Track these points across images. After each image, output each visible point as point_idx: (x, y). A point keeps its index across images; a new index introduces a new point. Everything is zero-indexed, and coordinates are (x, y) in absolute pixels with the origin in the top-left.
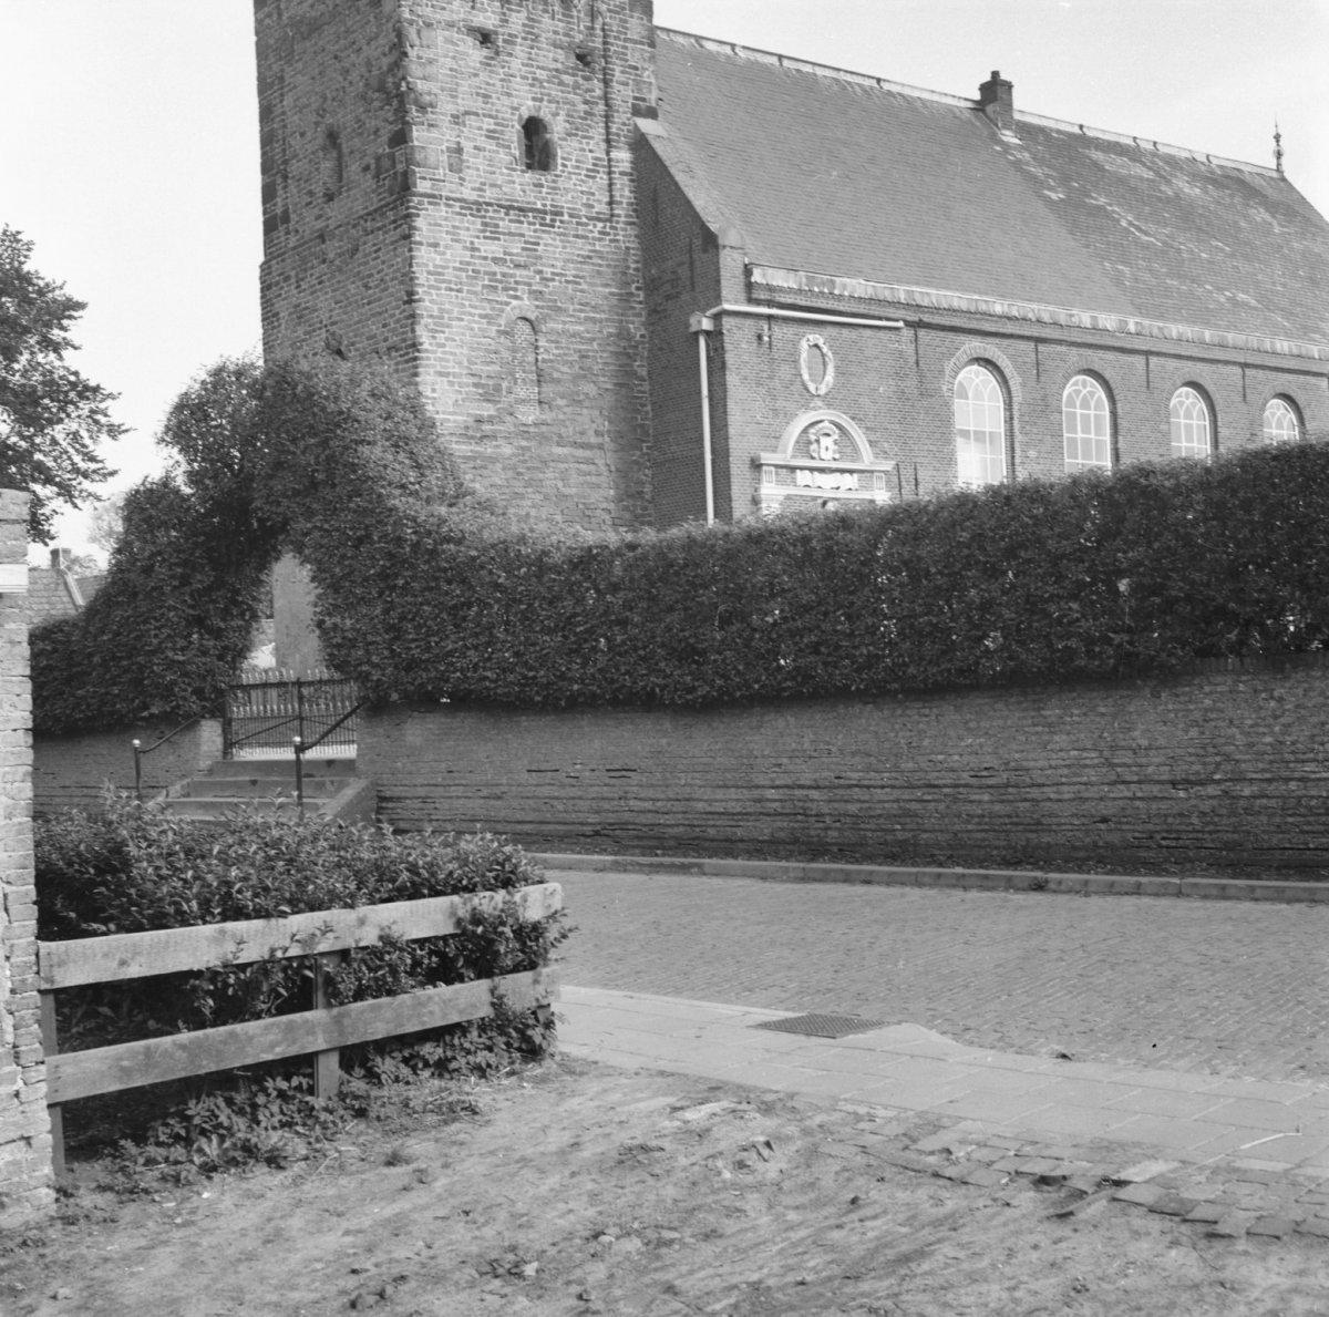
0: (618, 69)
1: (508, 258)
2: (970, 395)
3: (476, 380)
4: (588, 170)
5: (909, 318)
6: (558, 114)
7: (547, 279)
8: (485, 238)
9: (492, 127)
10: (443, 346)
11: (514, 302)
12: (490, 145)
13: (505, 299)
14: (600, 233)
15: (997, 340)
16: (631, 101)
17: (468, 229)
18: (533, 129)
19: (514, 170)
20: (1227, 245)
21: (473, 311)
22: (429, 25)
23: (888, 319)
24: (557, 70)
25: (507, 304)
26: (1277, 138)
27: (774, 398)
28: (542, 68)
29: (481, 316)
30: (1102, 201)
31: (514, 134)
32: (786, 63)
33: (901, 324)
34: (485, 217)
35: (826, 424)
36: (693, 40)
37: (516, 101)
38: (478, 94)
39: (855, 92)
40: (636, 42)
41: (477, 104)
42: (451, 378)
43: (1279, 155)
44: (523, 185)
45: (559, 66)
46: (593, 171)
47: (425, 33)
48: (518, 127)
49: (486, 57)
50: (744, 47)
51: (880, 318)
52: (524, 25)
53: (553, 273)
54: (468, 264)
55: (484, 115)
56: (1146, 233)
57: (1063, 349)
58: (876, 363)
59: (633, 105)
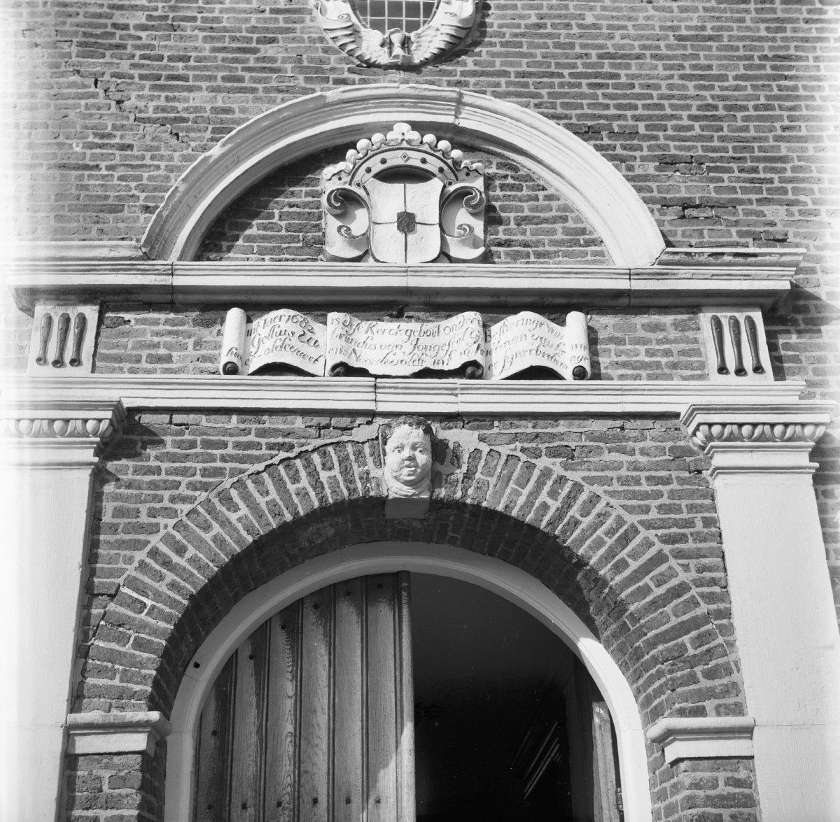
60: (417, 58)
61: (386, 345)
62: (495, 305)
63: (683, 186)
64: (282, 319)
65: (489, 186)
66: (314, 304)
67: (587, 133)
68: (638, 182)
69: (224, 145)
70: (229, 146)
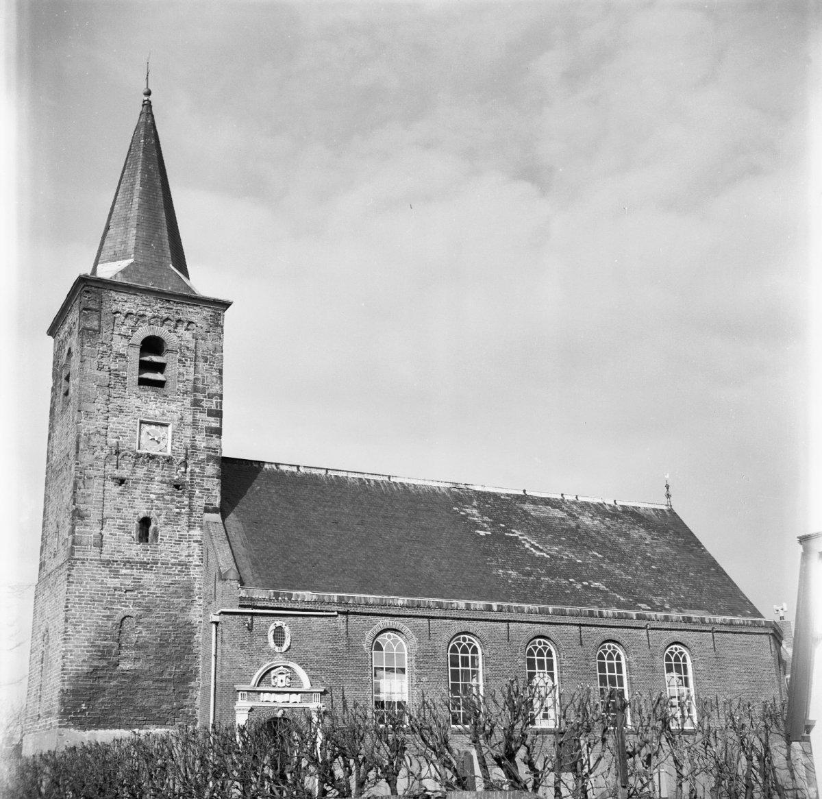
0: (197, 491)
1: (122, 587)
2: (384, 648)
3: (97, 648)
4: (176, 541)
5: (340, 610)
6: (160, 515)
7: (145, 596)
8: (110, 578)
9: (122, 524)
10: (80, 632)
11: (124, 608)
12: (119, 532)
13: (119, 607)
14: (179, 571)
15: (402, 619)
16: (204, 505)
17: (101, 574)
18: (145, 522)
19: (132, 543)
20: (600, 554)
21: (99, 614)
22: (89, 478)
23: (327, 611)
24: (162, 494)
25: (119, 609)
26: (667, 487)
27: (251, 655)
28: (154, 494)
29: (103, 616)
30: (517, 533)
31: (134, 527)
32: (330, 473)
33: (336, 613)
34: (111, 567)
35: (282, 668)
36: (274, 466)
37: (136, 510)
38: (115, 508)
39: (369, 485)
40: (209, 477)
41: (115, 514)
42: (82, 648)
43: (668, 496)
44: (135, 550)
45: (163, 491)
46: (179, 541)
47: (87, 482)
48: (136, 522)
49: (121, 491)
50: (305, 467)
51: (322, 611)
52: (145, 474)
53: (149, 593)
54: (99, 591)
55: (117, 518)
56: (541, 551)
57: (448, 621)
58: (319, 634)
59: (205, 507)
60: (283, 651)
61: (280, 698)
62: (291, 693)
63: (313, 673)
64: (267, 694)
65: (293, 677)
66: (271, 692)
67: (300, 665)
68: (307, 673)
69: (514, 533)
70: (513, 531)
